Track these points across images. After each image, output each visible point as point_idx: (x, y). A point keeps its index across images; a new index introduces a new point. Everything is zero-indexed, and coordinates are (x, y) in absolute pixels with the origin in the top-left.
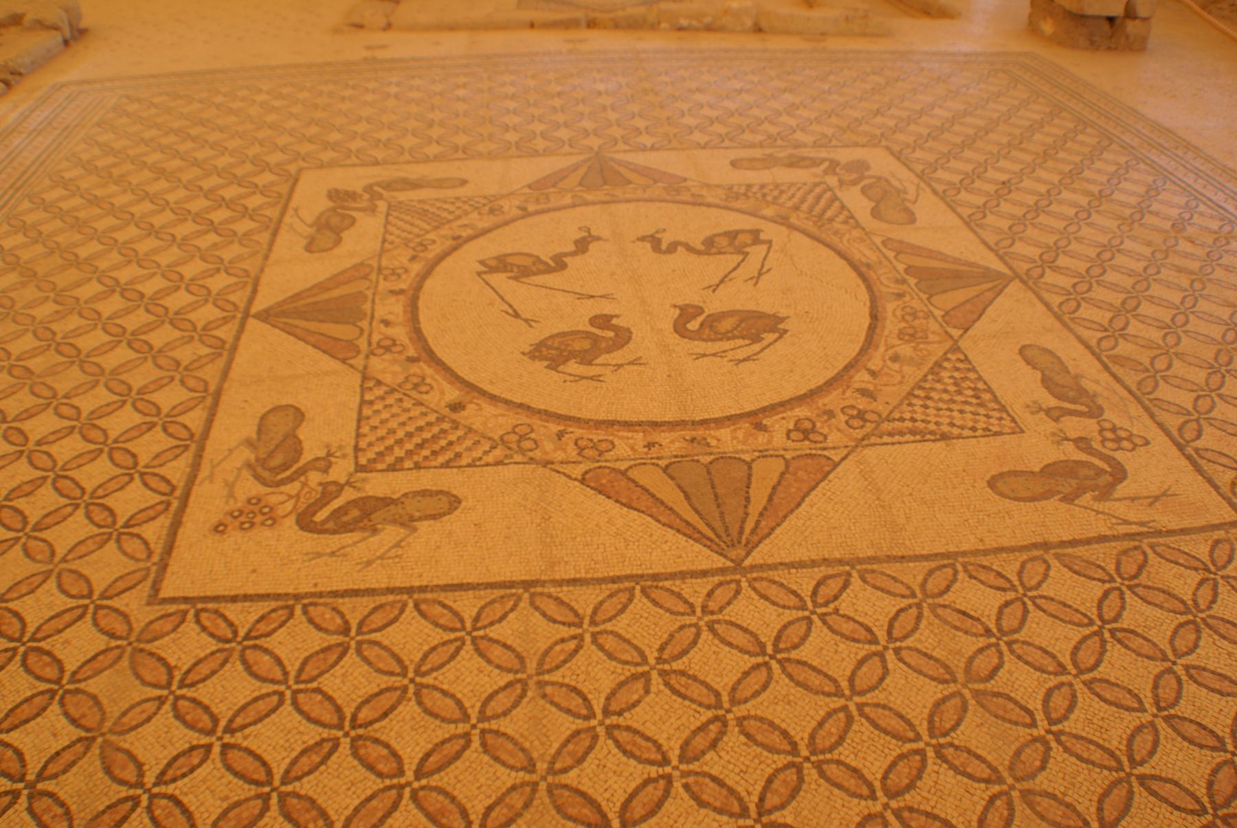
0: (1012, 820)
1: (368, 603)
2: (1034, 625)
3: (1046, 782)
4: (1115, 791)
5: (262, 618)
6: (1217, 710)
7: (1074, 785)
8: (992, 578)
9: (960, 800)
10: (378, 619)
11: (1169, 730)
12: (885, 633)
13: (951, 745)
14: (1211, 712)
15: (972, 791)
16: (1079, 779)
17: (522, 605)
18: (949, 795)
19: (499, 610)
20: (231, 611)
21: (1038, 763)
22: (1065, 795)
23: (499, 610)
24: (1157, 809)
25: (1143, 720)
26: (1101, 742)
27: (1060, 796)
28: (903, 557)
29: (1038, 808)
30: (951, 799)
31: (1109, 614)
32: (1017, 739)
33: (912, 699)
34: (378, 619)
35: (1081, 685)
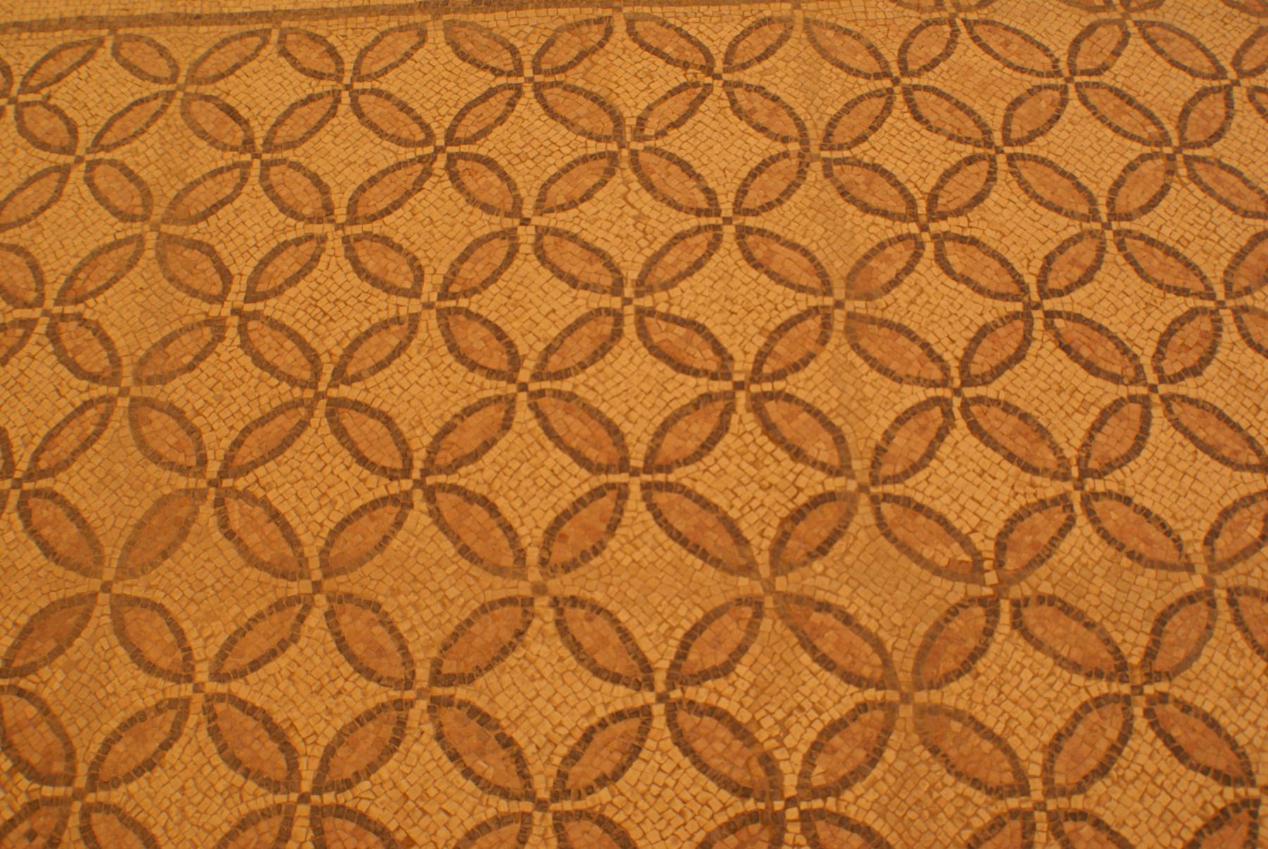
0: (94, 441)
1: (207, 35)
2: (328, 139)
3: (182, 390)
4: (281, 419)
5: (51, 55)
6: (546, 309)
7: (220, 399)
8: (314, 56)
9: (39, 404)
10: (756, 44)
11: (437, 333)
12: (92, 137)
13: (79, 317)
14: (533, 311)
15: (64, 390)
16: (236, 393)
17: (795, 34)
18: (29, 393)
19: (228, 57)
20: (334, 32)
21: (187, 359)
22: (198, 413)
23: (228, 57)
24: (327, 458)
25: (403, 312)
26: (309, 337)
27: (189, 414)
28: (198, 17)
29: (145, 430)
30: (27, 399)
31: (1215, 106)
32: (180, 318)
33: (67, 242)
34: (756, 44)
35: (339, 242)
